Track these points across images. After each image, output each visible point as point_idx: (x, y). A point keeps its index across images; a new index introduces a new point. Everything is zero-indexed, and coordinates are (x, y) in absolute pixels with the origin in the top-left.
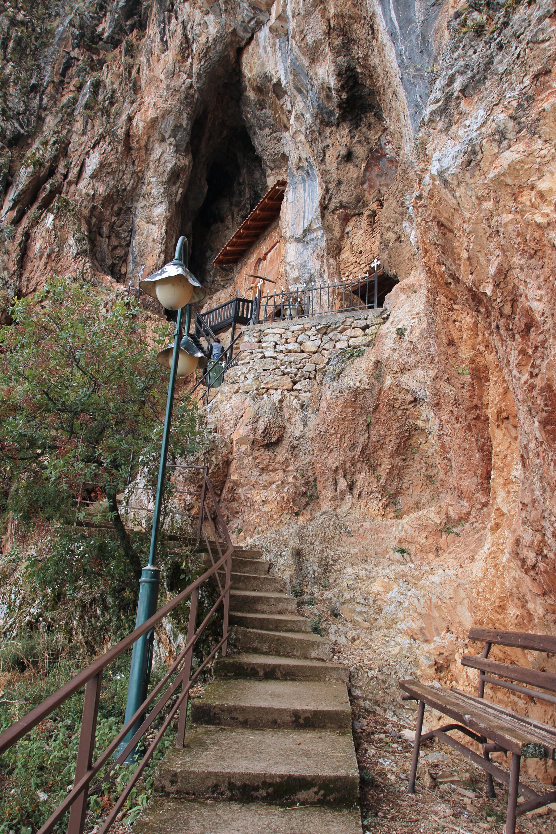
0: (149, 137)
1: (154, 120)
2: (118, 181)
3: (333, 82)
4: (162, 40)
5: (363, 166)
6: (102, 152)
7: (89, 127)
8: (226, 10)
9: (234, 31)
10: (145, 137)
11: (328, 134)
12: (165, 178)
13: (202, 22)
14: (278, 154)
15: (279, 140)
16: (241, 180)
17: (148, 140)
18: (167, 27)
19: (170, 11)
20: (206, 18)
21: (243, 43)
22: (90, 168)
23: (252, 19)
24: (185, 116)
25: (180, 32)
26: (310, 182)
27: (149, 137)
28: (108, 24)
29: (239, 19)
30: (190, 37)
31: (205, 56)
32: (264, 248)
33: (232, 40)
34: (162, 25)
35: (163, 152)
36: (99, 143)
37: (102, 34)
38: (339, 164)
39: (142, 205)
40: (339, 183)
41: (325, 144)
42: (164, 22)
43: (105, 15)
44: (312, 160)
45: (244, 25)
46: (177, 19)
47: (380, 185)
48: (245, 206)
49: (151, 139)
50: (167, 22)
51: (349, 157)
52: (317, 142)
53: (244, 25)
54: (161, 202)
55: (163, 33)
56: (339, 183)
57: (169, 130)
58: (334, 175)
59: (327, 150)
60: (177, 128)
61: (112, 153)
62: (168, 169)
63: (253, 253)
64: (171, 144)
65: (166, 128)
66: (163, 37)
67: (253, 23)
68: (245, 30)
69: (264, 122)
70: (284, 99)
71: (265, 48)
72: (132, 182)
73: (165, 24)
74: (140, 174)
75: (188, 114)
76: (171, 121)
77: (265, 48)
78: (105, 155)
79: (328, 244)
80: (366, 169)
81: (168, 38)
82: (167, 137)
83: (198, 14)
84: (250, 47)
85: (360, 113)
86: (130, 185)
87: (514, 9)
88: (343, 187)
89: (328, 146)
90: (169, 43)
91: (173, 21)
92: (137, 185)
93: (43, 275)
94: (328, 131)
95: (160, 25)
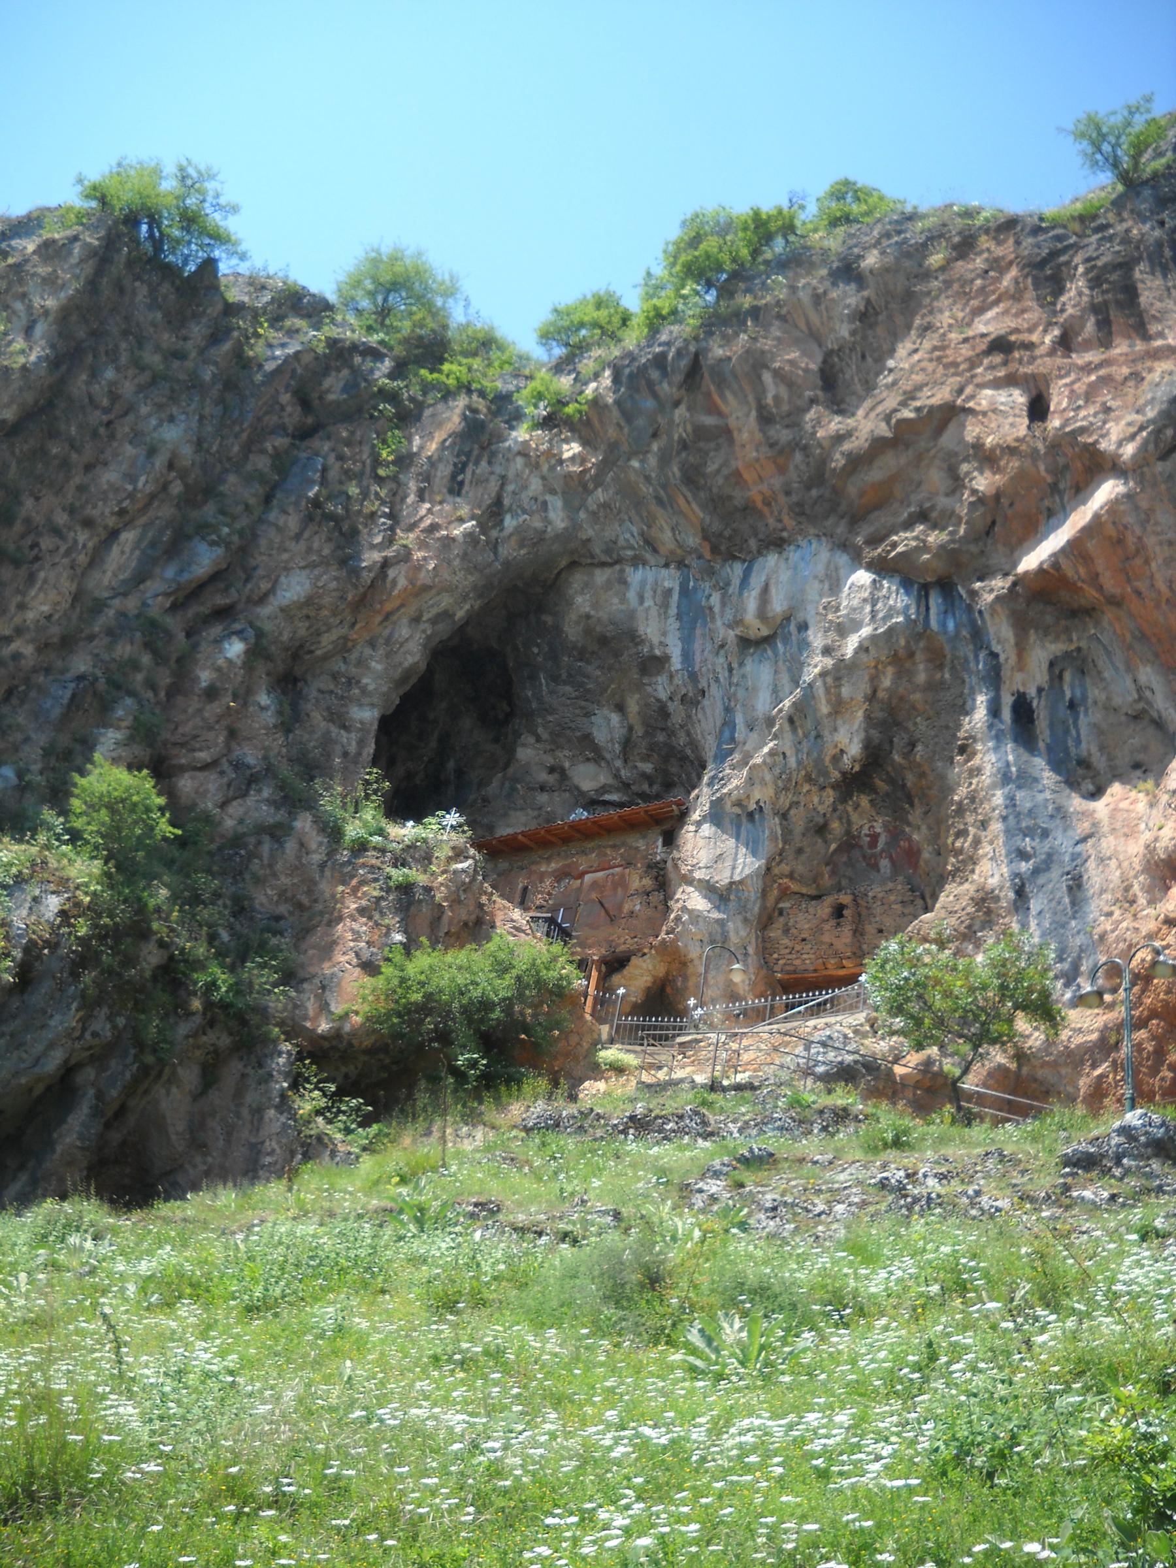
0: (402, 605)
1: (426, 588)
3: (854, 749)
4: (453, 476)
5: (833, 846)
6: (320, 584)
7: (306, 535)
9: (589, 540)
10: (398, 603)
12: (397, 674)
13: (541, 499)
17: (398, 609)
18: (471, 467)
19: (483, 448)
20: (548, 497)
22: (288, 595)
23: (632, 548)
24: (467, 607)
25: (493, 486)
26: (750, 826)
27: (402, 605)
28: (341, 384)
29: (609, 534)
30: (506, 502)
31: (534, 545)
32: (583, 863)
34: (464, 458)
35: (411, 637)
37: (328, 391)
38: (807, 829)
39: (323, 686)
42: (468, 454)
43: (338, 370)
44: (767, 809)
46: (490, 463)
50: (473, 459)
51: (821, 830)
55: (460, 468)
58: (798, 841)
60: (446, 615)
62: (406, 664)
63: (549, 860)
64: (424, 631)
67: (630, 553)
68: (608, 551)
69: (570, 675)
71: (641, 599)
73: (468, 460)
74: (350, 644)
76: (446, 601)
77: (641, 599)
80: (836, 851)
81: (467, 482)
83: (535, 485)
84: (601, 576)
87: (682, 1131)
88: (803, 857)
90: (466, 488)
91: (484, 463)
93: (210, 728)
95: (458, 456)
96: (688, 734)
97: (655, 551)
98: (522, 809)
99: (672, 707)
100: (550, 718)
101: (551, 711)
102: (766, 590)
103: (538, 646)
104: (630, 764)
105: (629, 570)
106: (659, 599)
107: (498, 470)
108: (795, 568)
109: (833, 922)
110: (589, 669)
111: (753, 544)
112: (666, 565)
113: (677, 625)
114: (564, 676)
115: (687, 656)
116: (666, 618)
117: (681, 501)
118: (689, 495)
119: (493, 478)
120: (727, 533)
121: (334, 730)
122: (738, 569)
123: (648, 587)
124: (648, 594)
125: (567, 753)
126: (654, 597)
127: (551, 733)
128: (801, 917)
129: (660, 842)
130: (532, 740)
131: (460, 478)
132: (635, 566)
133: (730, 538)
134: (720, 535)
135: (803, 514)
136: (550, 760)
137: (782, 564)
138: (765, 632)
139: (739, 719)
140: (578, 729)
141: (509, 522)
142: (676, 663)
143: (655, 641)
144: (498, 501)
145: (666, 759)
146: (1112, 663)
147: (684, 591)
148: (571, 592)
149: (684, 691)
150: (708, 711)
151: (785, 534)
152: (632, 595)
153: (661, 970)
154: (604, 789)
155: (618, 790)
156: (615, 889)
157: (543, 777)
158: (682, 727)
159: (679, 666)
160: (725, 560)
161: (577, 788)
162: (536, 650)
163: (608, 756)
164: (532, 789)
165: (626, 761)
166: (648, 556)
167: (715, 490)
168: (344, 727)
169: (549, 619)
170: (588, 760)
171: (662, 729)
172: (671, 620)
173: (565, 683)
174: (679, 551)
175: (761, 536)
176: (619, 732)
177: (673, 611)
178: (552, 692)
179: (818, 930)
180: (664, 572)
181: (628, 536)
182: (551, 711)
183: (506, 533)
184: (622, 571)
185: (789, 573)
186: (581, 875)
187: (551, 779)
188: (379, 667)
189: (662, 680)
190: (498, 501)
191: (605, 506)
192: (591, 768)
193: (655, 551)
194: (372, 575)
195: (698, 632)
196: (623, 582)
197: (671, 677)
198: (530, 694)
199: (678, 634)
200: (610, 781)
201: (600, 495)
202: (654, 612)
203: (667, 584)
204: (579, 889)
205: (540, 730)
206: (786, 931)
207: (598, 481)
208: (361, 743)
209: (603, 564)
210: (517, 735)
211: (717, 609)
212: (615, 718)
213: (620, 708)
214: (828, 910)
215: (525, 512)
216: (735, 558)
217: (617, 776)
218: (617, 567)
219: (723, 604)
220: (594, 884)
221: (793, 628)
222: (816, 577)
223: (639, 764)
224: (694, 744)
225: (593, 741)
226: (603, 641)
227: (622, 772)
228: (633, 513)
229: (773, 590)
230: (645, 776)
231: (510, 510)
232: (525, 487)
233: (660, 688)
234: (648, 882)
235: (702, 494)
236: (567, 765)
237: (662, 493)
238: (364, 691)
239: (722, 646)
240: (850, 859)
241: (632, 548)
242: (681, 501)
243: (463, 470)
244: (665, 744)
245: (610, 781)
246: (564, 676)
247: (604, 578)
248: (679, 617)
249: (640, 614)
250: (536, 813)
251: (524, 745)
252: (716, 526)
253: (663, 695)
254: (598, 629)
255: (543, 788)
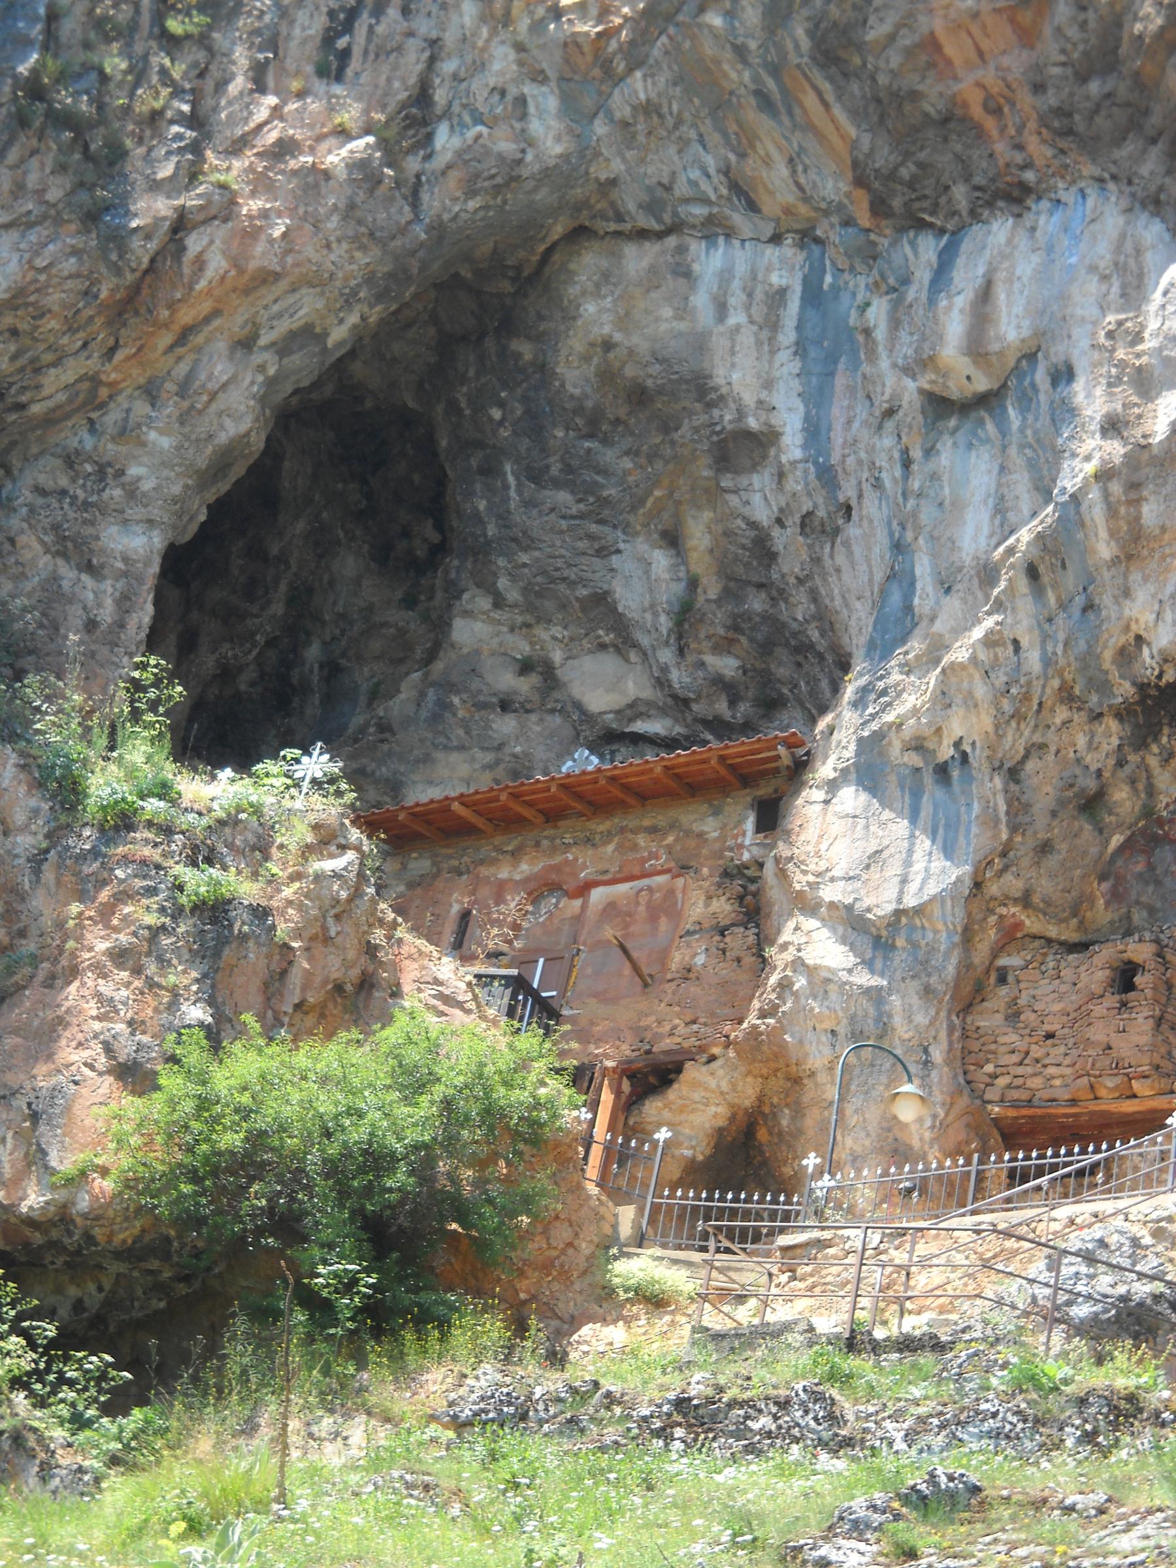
0: (216, 313)
1: (267, 278)
2: (22, 370)
4: (328, 40)
5: (1116, 840)
6: (40, 263)
8: (625, 124)
9: (613, 182)
10: (207, 306)
11: (1058, 721)
12: (202, 462)
13: (513, 91)
14: (572, 584)
15: (604, 552)
16: (274, 550)
17: (207, 320)
18: (364, 21)
20: (529, 89)
21: (612, 227)
23: (706, 201)
24: (353, 319)
25: (413, 61)
27: (216, 313)
29: (656, 170)
30: (440, 96)
31: (498, 189)
32: (587, 863)
33: (588, 200)
35: (232, 380)
36: (30, 225)
38: (1062, 803)
39: (44, 480)
40: (1045, 848)
41: (1037, 738)
44: (978, 758)
45: (660, 192)
47: (1138, 902)
48: (253, 634)
49: (216, 323)
52: (1023, 725)
53: (660, 192)
54: (150, 522)
56: (1045, 848)
57: (284, 326)
59: (1034, 753)
60: (308, 335)
61: (70, 284)
62: (223, 438)
63: (516, 855)
64: (261, 368)
65: (279, 315)
66: (340, 34)
67: (699, 211)
68: (652, 207)
69: (568, 469)
70: (744, 481)
71: (722, 310)
72: (62, 397)
74: (104, 392)
75: (363, 318)
77: (722, 310)
78: (43, 278)
79: (959, 973)
80: (1121, 849)
81: (357, 52)
82: (263, 341)
85: (1165, 721)
86: (50, 404)
88: (1052, 861)
89: (1043, 746)
90: (354, 64)
92: (67, 416)
94: (1062, 714)
96: (814, 596)
97: (753, 207)
98: (461, 748)
99: (780, 539)
100: (524, 558)
101: (526, 541)
102: (985, 294)
103: (502, 405)
104: (691, 658)
105: (696, 247)
106: (758, 311)
107: (424, 27)
108: (1050, 249)
109: (1112, 1000)
110: (608, 456)
111: (960, 194)
112: (776, 239)
113: (795, 366)
114: (555, 470)
115: (814, 431)
116: (773, 353)
117: (810, 100)
118: (826, 87)
119: (412, 44)
120: (905, 173)
121: (67, 573)
122: (928, 248)
123: (736, 284)
124: (736, 299)
125: (557, 631)
126: (748, 307)
127: (525, 591)
128: (1045, 987)
129: (750, 824)
130: (484, 603)
131: (341, 43)
132: (710, 238)
133: (911, 184)
134: (892, 176)
135: (1069, 132)
136: (521, 647)
137: (1023, 242)
138: (982, 384)
139: (923, 567)
140: (582, 582)
141: (445, 140)
142: (792, 446)
143: (749, 399)
144: (423, 96)
145: (766, 648)
146: (126, 420)
147: (813, 295)
148: (573, 291)
149: (807, 506)
150: (858, 551)
151: (1030, 176)
152: (701, 300)
153: (748, 1093)
154: (635, 710)
155: (663, 711)
156: (653, 918)
157: (507, 680)
158: (800, 581)
159: (798, 454)
160: (901, 230)
161: (578, 706)
162: (496, 414)
163: (645, 641)
164: (484, 706)
165: (681, 652)
166: (738, 219)
167: (883, 79)
168: (89, 568)
169: (525, 350)
170: (603, 647)
171: (760, 586)
172: (784, 355)
173: (557, 484)
174: (803, 210)
175: (978, 180)
176: (670, 591)
177: (788, 336)
178: (529, 504)
179: (1080, 1017)
180: (771, 253)
181: (695, 174)
182: (526, 541)
183: (438, 163)
184: (682, 250)
185: (1036, 259)
186: (584, 889)
187: (524, 686)
188: (165, 442)
189: (761, 480)
190: (423, 96)
191: (649, 109)
192: (608, 663)
193: (753, 207)
194: (152, 246)
195: (840, 381)
196: (685, 273)
197: (781, 476)
198: (482, 505)
199: (796, 385)
200: (647, 692)
201: (639, 86)
202: (747, 338)
203: (775, 279)
204: (578, 919)
205: (503, 583)
206: (1013, 1016)
207: (635, 56)
208: (125, 602)
209: (642, 235)
210: (454, 591)
211: (880, 334)
212: (661, 560)
213: (672, 540)
214: (1102, 975)
215: (478, 119)
216: (922, 225)
217: (661, 682)
218: (672, 241)
219: (895, 323)
220: (610, 909)
221: (1041, 376)
222: (1093, 269)
223: (709, 659)
224: (825, 619)
225: (613, 609)
226: (639, 396)
227: (675, 675)
228: (707, 127)
229: (1001, 295)
230: (719, 683)
231: (447, 114)
232: (480, 66)
233: (757, 499)
234: (723, 907)
235: (855, 87)
236: (557, 656)
237: (771, 84)
238: (132, 492)
239: (890, 413)
240: (1151, 867)
241: (706, 201)
242: (810, 100)
243: (348, 26)
244: (765, 617)
245: (647, 692)
246: (555, 470)
247: (645, 263)
248: (800, 349)
249: (719, 343)
250: (489, 757)
251: (467, 614)
252: (884, 158)
253: (762, 514)
254: (630, 371)
255: (505, 706)
